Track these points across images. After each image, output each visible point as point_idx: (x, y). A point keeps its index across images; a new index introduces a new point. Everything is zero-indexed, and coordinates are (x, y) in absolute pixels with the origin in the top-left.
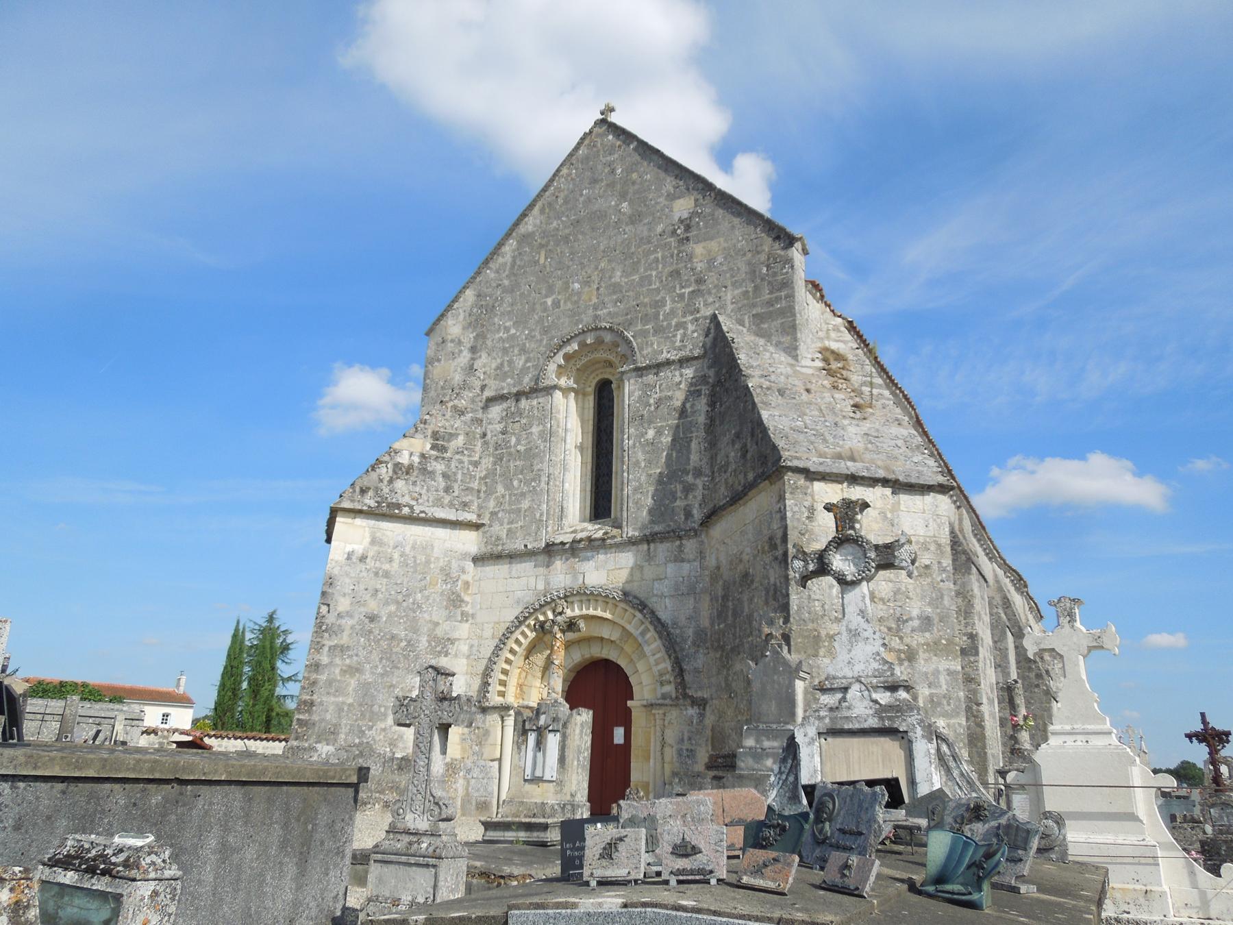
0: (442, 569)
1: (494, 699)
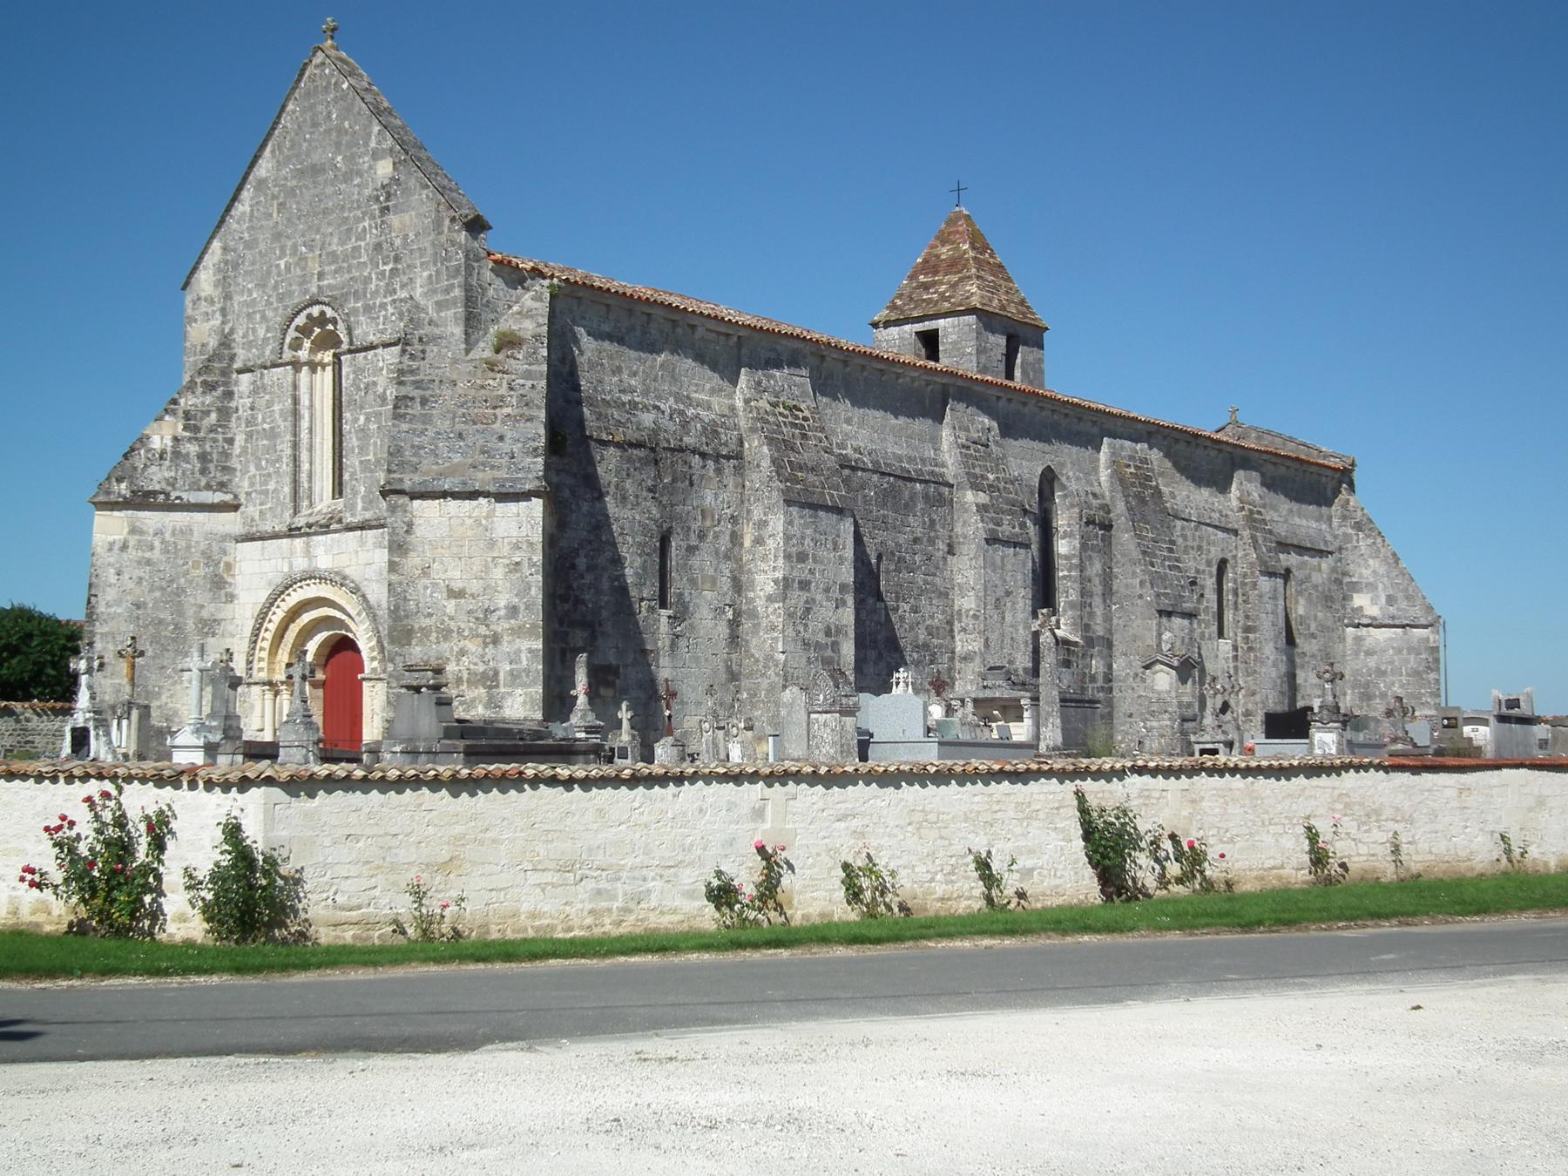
0: (203, 553)
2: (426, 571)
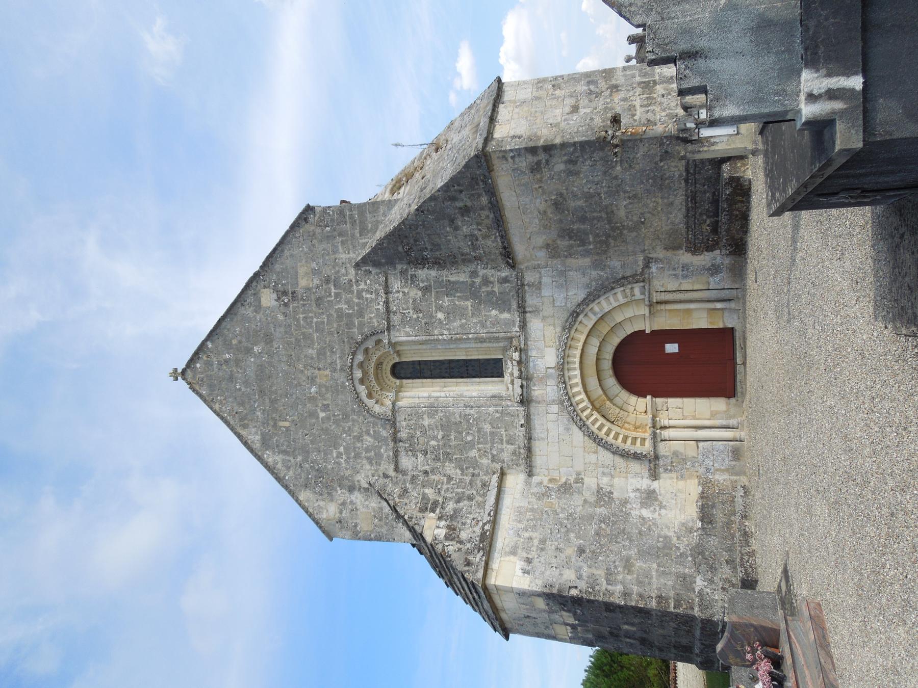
1: (648, 447)
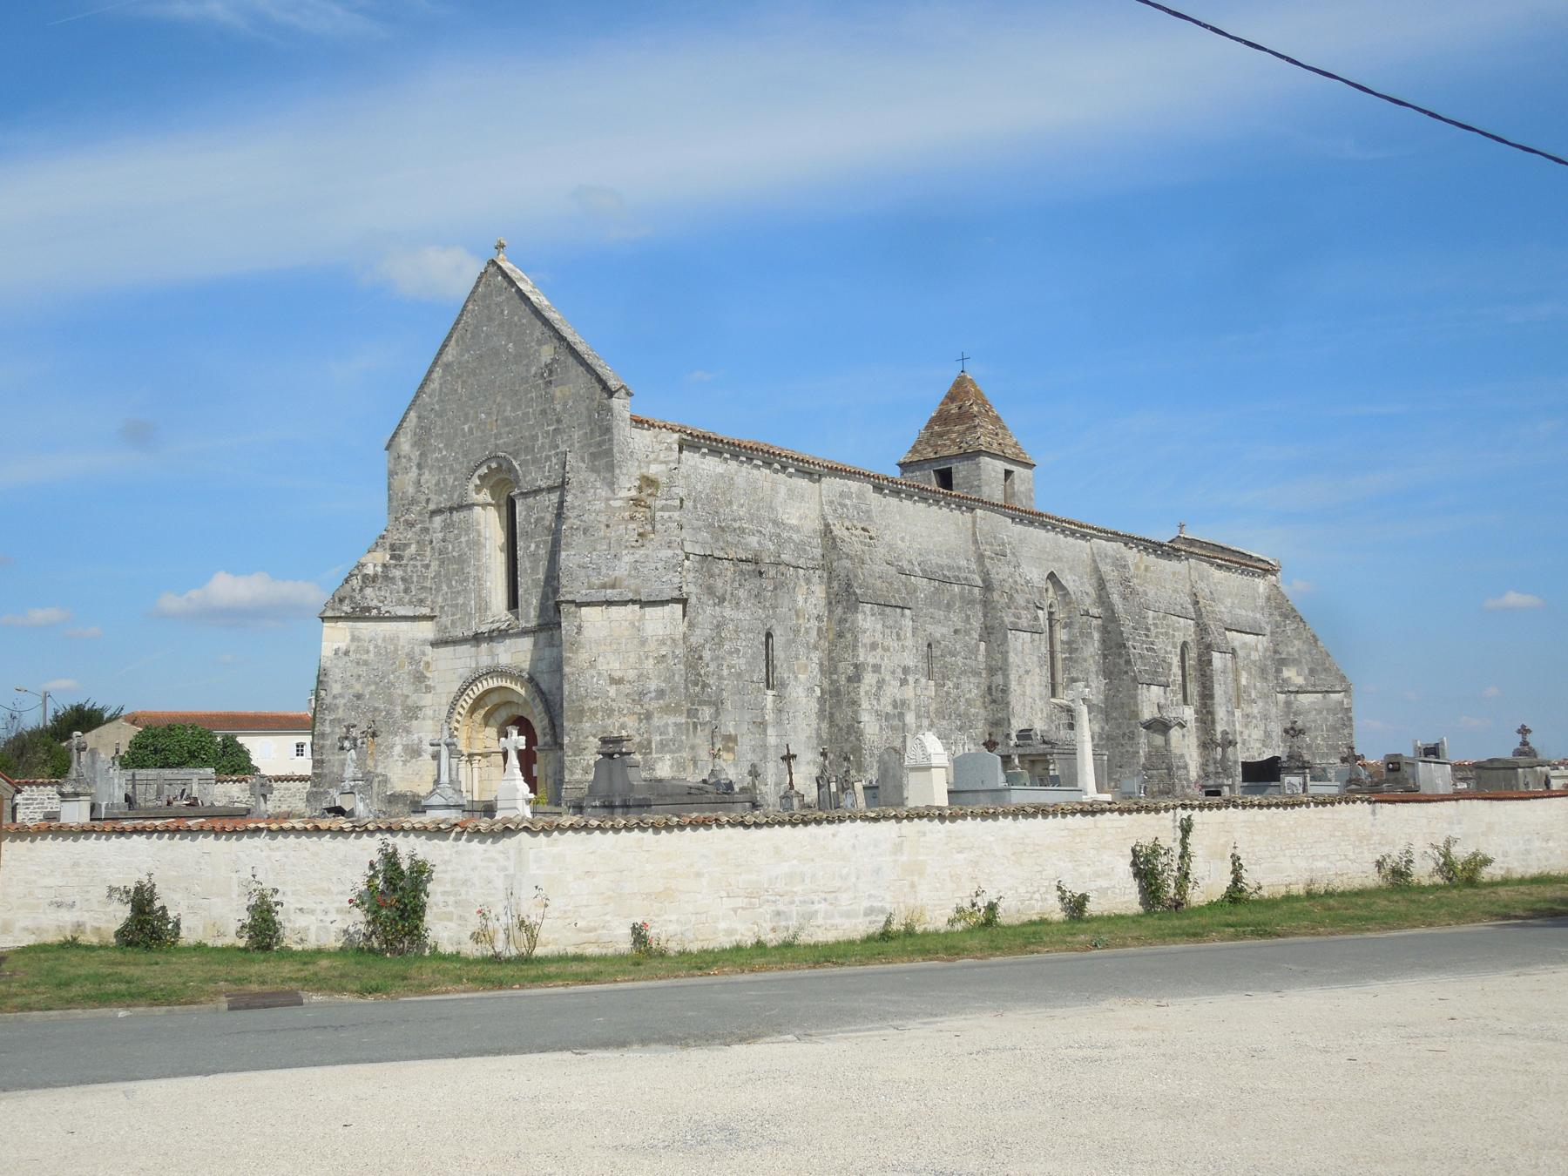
2: (593, 664)
